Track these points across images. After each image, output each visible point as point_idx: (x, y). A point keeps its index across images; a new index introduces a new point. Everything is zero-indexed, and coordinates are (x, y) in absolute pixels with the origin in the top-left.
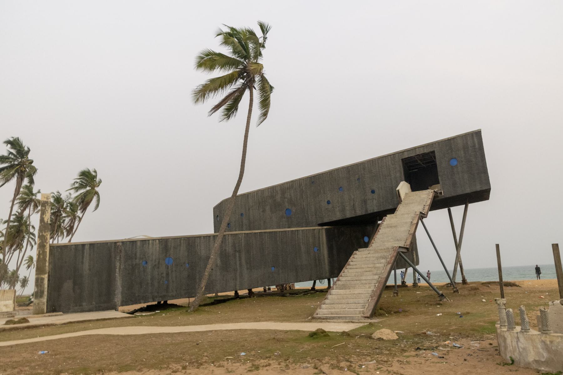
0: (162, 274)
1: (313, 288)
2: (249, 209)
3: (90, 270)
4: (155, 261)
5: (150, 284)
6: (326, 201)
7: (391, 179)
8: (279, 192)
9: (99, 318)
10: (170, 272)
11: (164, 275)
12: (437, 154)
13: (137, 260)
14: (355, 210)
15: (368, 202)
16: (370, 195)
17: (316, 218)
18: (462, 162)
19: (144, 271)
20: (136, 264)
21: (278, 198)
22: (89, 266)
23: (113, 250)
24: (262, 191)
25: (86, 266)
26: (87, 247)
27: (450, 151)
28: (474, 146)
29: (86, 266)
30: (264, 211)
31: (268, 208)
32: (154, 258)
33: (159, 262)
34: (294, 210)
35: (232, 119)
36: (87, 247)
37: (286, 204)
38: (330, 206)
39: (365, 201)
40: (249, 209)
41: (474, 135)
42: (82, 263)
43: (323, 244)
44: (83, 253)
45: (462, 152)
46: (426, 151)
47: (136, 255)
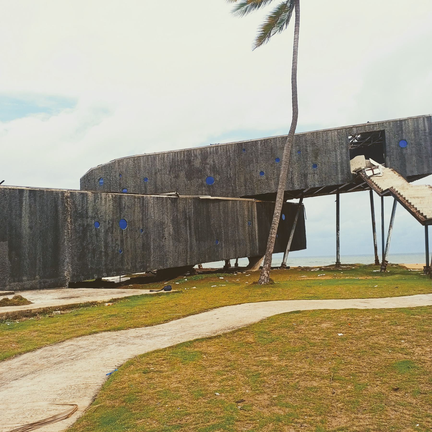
0: (117, 240)
1: (283, 265)
2: (156, 173)
3: (31, 228)
4: (109, 223)
5: (103, 254)
6: (259, 171)
7: (336, 155)
8: (199, 157)
9: (76, 299)
10: (124, 238)
11: (119, 242)
12: (387, 134)
13: (89, 220)
14: (293, 184)
15: (309, 176)
16: (311, 170)
17: (246, 189)
18: (412, 144)
19: (97, 235)
20: (88, 225)
21: (197, 163)
22: (31, 222)
23: (60, 202)
24: (176, 154)
25: (26, 222)
26: (26, 194)
27: (400, 132)
28: (425, 130)
29: (26, 222)
30: (177, 177)
31: (182, 174)
32: (108, 218)
33: (113, 224)
34: (218, 178)
35: (261, 46)
36: (26, 194)
37: (208, 171)
38: (264, 177)
39: (304, 175)
40: (156, 173)
41: (426, 119)
42: (20, 216)
43: (255, 218)
44: (21, 203)
45: (413, 135)
46: (376, 129)
47: (87, 213)
